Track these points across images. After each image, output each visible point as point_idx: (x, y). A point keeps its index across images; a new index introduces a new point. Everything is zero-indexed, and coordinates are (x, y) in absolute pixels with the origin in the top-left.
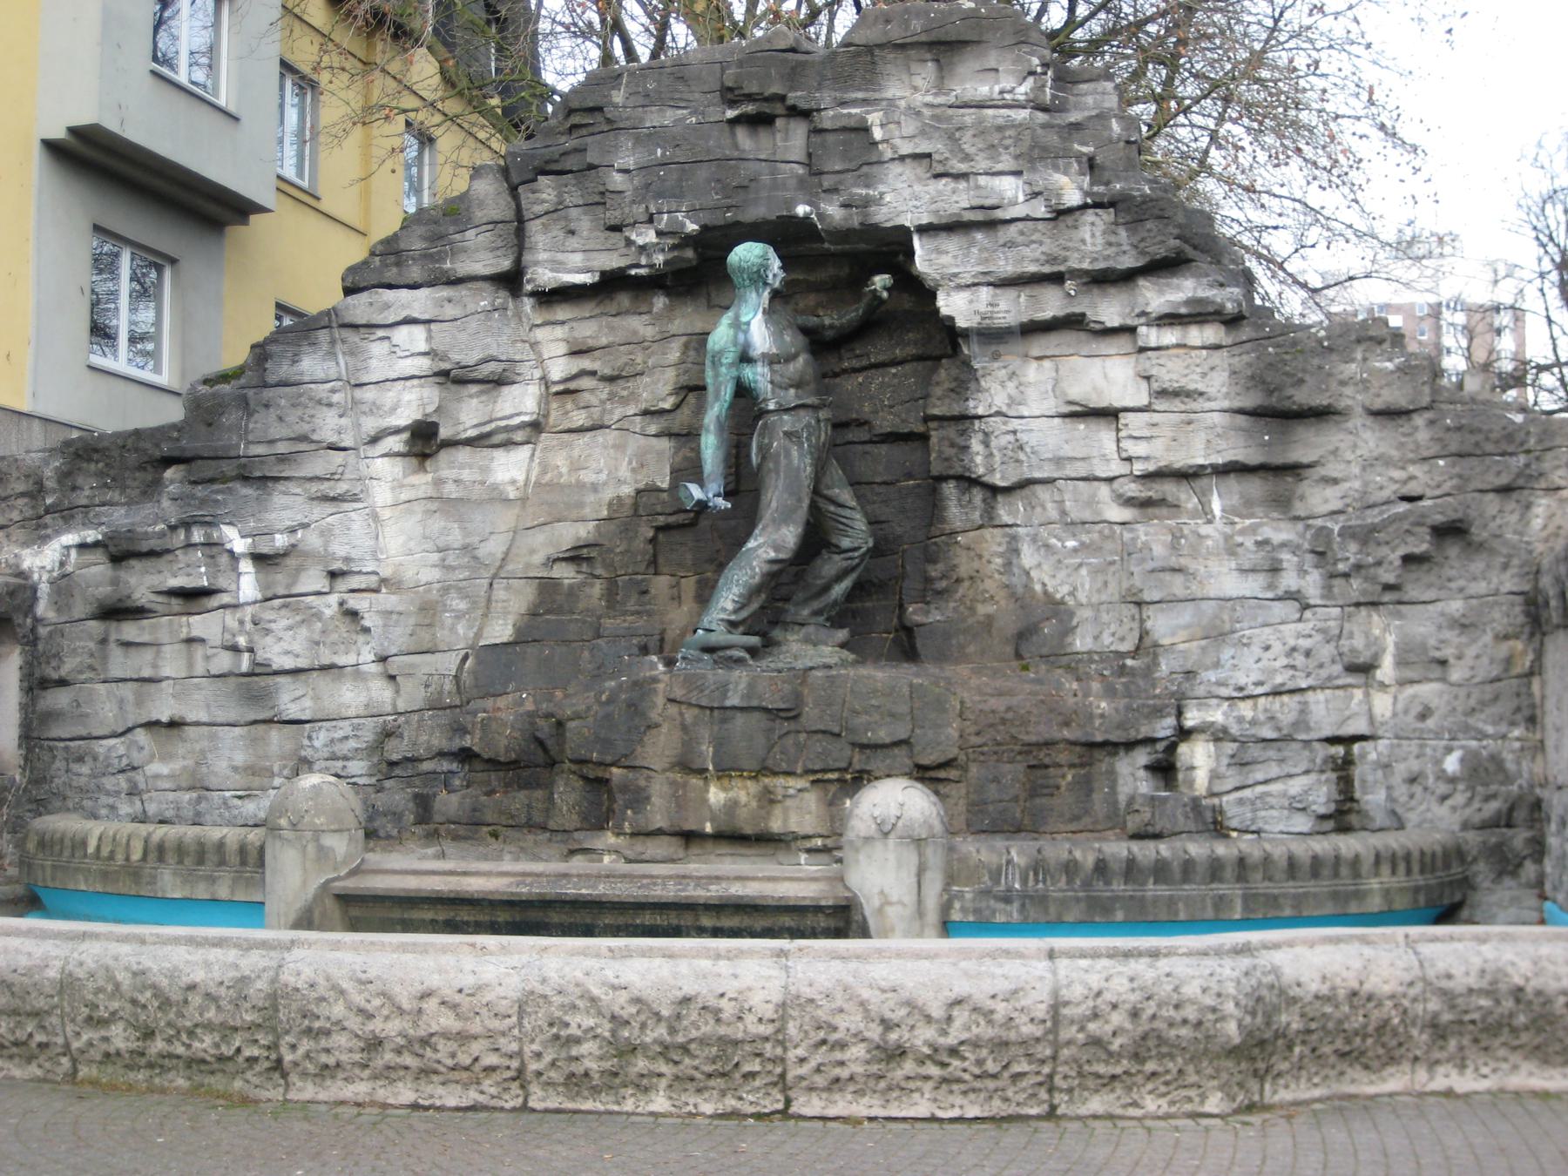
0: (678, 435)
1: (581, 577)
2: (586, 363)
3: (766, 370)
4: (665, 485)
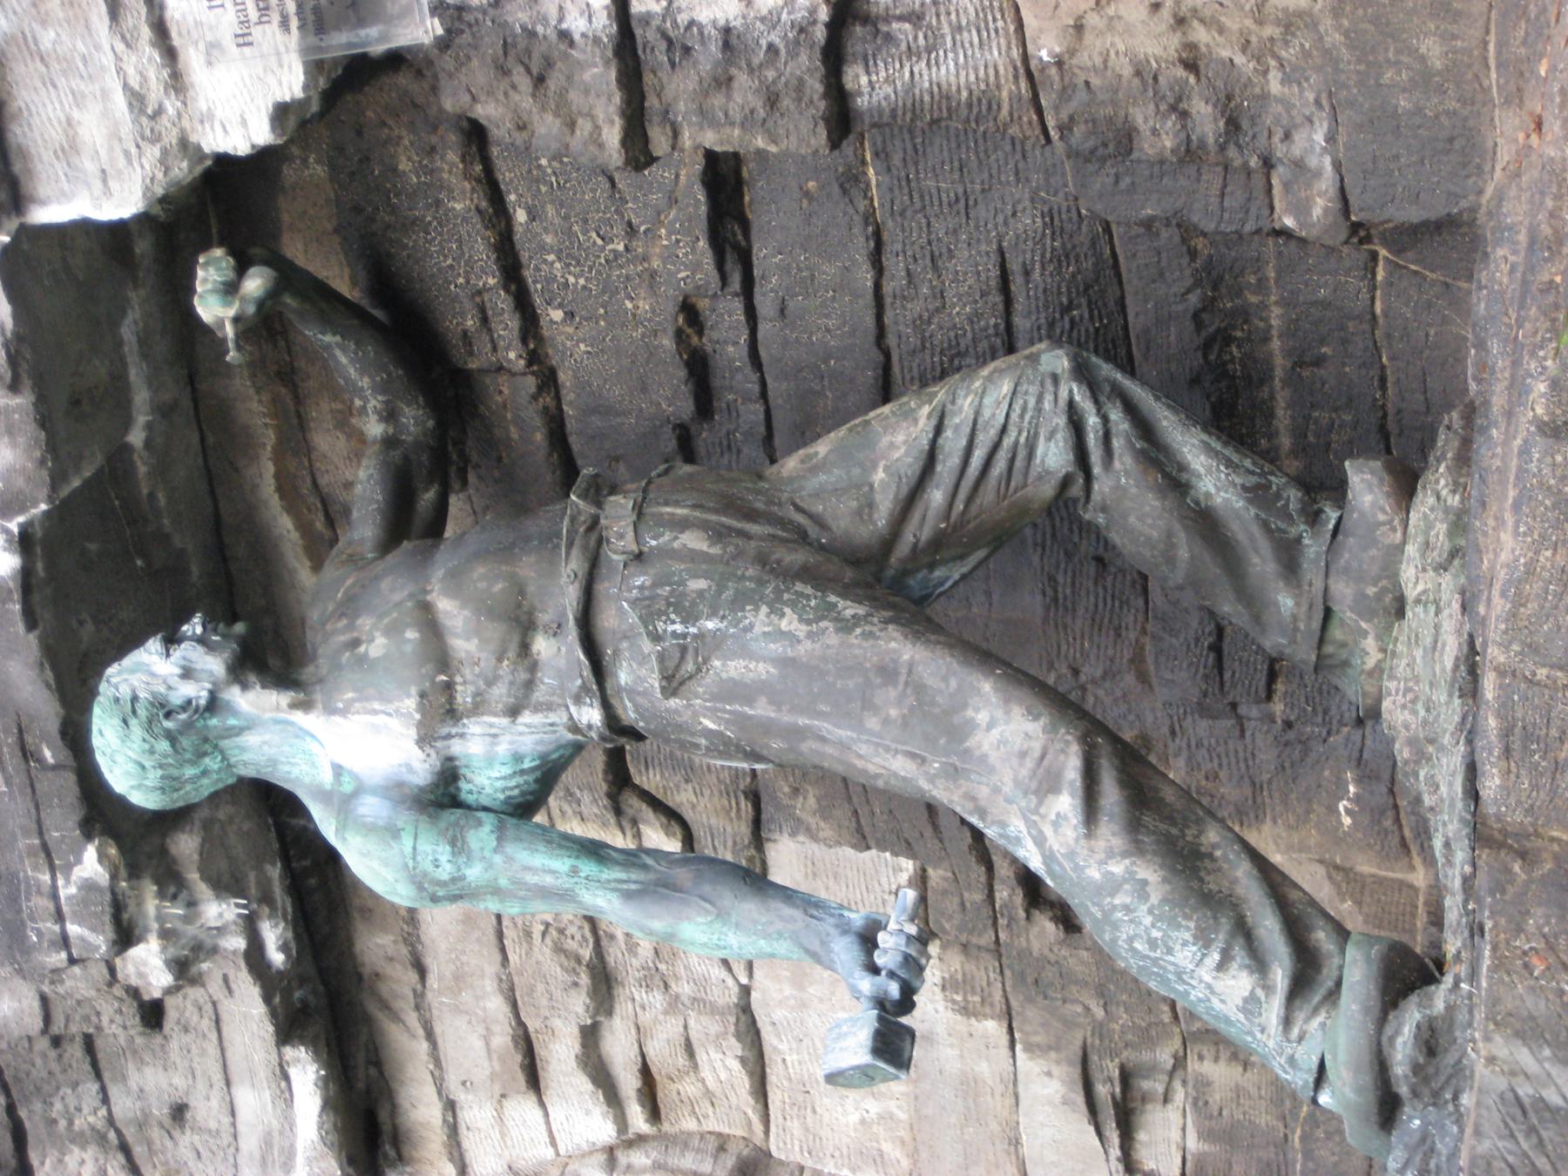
0: (757, 824)
1: (1179, 1095)
2: (560, 1054)
3: (473, 727)
4: (908, 866)
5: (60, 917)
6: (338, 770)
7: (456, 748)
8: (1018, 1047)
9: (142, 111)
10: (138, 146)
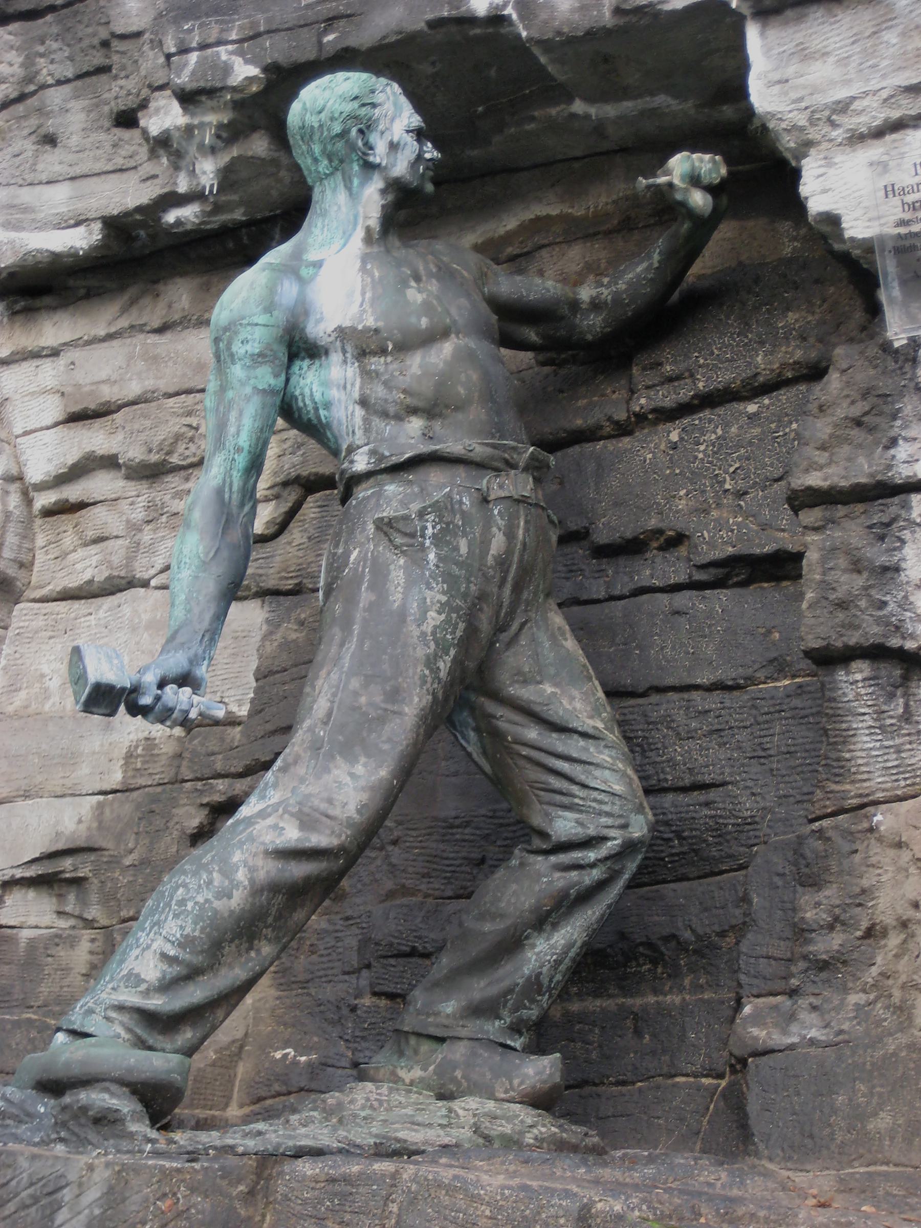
0: (276, 593)
3: (352, 371)
4: (243, 711)
5: (203, 47)
6: (318, 265)
7: (336, 357)
8: (101, 798)
9: (834, 111)
10: (806, 108)
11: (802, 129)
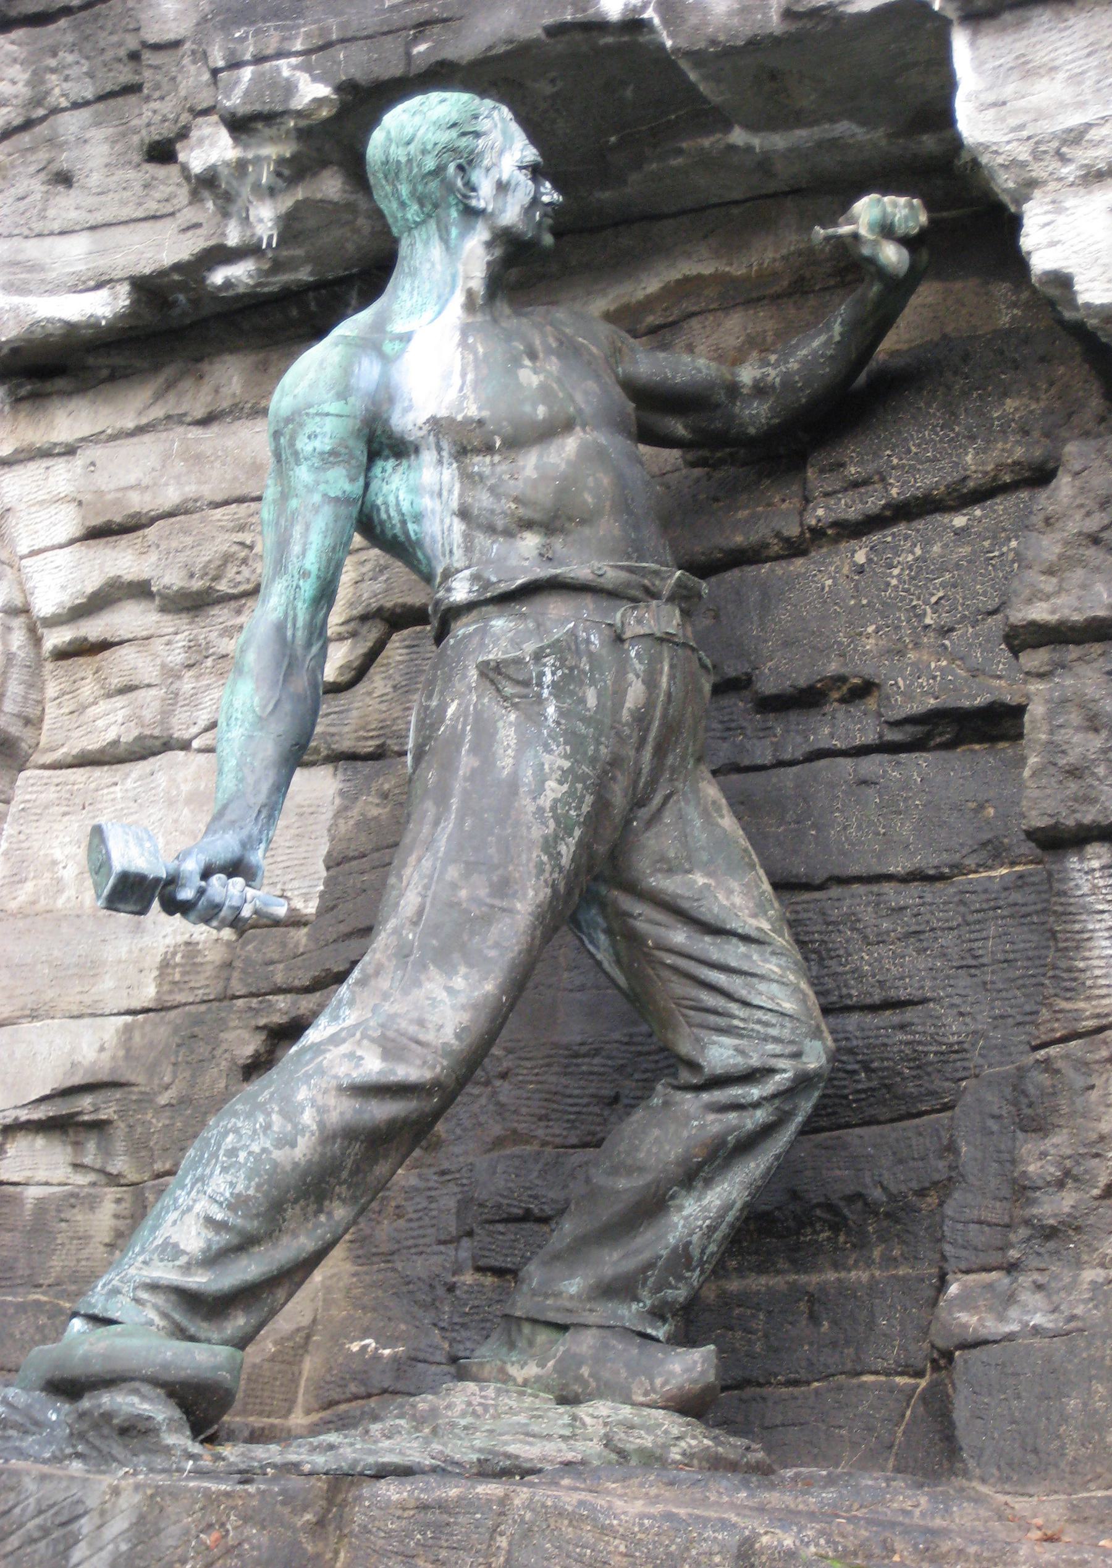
0: (352, 757)
3: (449, 474)
4: (310, 908)
5: (259, 60)
6: (406, 338)
7: (428, 456)
8: (129, 1019)
9: (1064, 142)
10: (1029, 138)
11: (1023, 165)
